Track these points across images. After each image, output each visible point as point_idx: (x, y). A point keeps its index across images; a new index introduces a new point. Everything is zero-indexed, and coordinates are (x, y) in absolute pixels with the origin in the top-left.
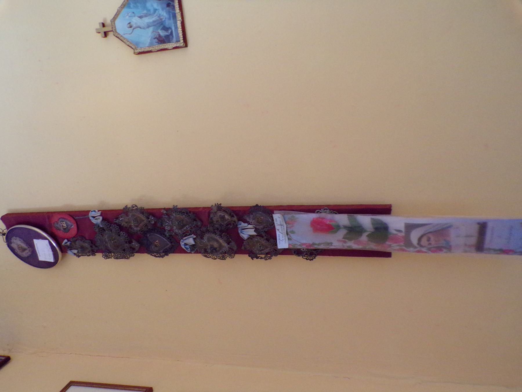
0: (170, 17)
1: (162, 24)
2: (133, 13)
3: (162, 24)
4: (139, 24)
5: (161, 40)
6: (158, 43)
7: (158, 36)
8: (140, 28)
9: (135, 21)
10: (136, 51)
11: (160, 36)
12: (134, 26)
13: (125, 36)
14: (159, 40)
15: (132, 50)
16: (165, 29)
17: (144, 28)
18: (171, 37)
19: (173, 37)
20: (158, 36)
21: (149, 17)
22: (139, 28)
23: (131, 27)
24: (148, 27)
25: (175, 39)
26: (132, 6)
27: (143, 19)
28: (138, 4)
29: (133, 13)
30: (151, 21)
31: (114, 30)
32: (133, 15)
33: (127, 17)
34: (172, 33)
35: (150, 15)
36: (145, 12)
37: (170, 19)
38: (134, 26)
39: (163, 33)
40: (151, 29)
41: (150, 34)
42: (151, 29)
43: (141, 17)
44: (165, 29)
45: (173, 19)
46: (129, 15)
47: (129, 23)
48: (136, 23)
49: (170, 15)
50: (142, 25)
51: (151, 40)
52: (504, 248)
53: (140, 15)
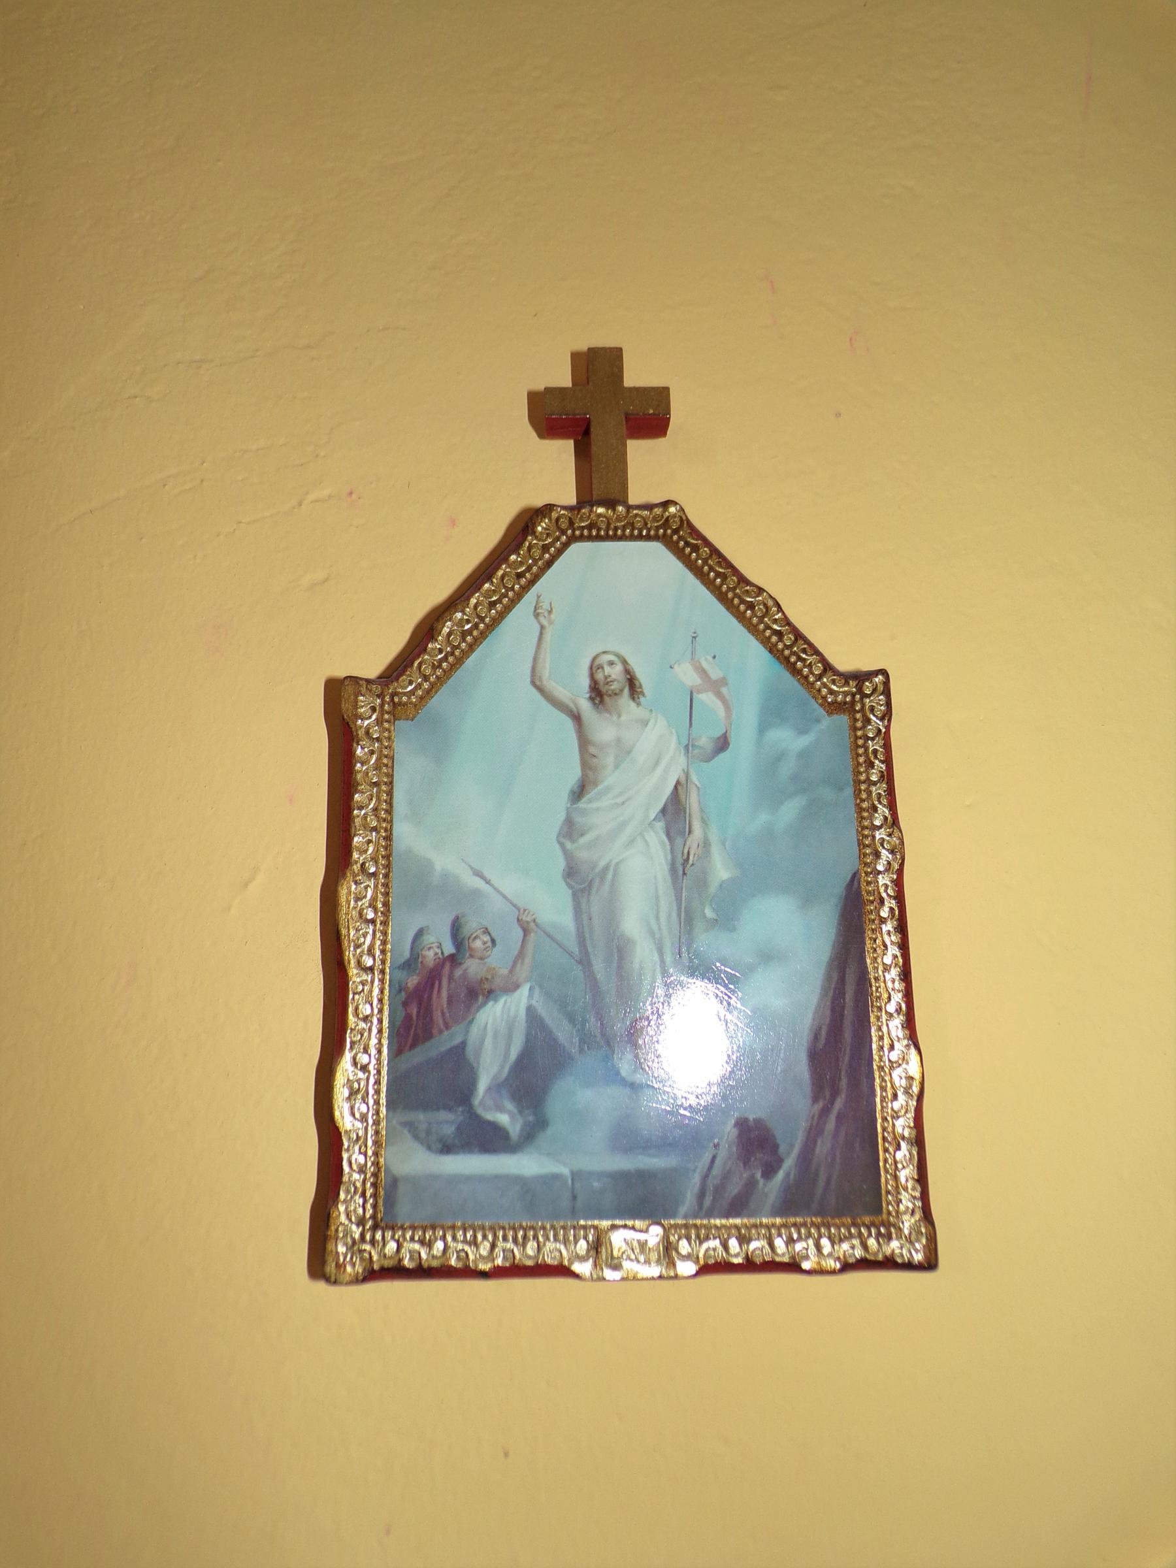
0: (647, 1146)
1: (586, 1041)
2: (723, 744)
3: (586, 1041)
4: (611, 778)
5: (430, 1001)
6: (409, 965)
7: (472, 968)
8: (580, 792)
9: (648, 751)
10: (364, 703)
11: (478, 993)
12: (603, 730)
13: (519, 621)
14: (432, 977)
15: (372, 669)
16: (531, 1080)
17: (570, 830)
18: (447, 1122)
19: (447, 1148)
20: (472, 968)
21: (666, 903)
22: (576, 773)
23: (598, 694)
24: (581, 880)
25: (414, 1161)
26: (786, 738)
27: (656, 839)
28: (790, 811)
29: (723, 744)
30: (632, 924)
31: (603, 508)
32: (705, 739)
33: (687, 675)
34: (489, 1139)
35: (687, 920)
36: (721, 870)
37: (626, 1137)
38: (603, 730)
39: (494, 1032)
40: (553, 908)
41: (511, 885)
42: (553, 908)
43: (675, 811)
44: (531, 1080)
45: (623, 1179)
46: (707, 698)
47: (632, 685)
48: (624, 751)
49: (664, 1145)
50: (600, 815)
51: (448, 887)
52: (509, 897)
53: (693, 801)
